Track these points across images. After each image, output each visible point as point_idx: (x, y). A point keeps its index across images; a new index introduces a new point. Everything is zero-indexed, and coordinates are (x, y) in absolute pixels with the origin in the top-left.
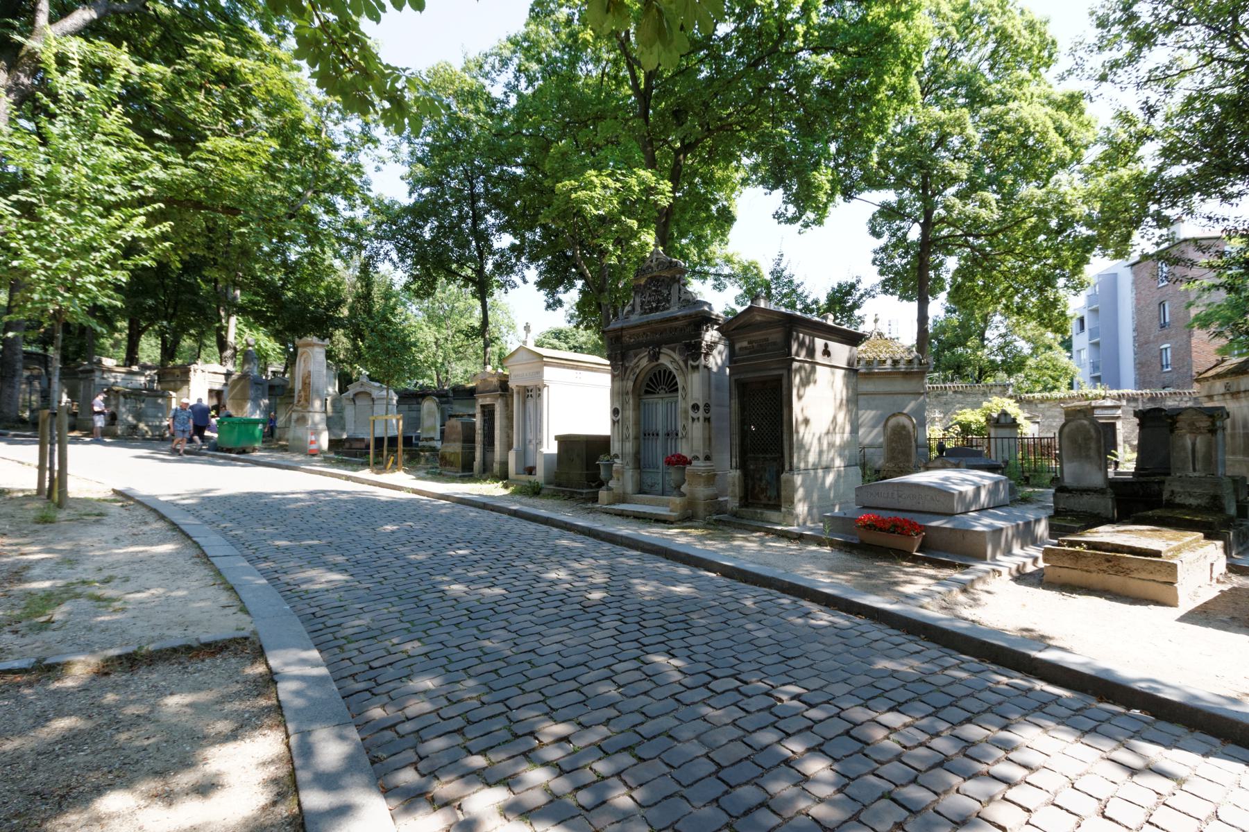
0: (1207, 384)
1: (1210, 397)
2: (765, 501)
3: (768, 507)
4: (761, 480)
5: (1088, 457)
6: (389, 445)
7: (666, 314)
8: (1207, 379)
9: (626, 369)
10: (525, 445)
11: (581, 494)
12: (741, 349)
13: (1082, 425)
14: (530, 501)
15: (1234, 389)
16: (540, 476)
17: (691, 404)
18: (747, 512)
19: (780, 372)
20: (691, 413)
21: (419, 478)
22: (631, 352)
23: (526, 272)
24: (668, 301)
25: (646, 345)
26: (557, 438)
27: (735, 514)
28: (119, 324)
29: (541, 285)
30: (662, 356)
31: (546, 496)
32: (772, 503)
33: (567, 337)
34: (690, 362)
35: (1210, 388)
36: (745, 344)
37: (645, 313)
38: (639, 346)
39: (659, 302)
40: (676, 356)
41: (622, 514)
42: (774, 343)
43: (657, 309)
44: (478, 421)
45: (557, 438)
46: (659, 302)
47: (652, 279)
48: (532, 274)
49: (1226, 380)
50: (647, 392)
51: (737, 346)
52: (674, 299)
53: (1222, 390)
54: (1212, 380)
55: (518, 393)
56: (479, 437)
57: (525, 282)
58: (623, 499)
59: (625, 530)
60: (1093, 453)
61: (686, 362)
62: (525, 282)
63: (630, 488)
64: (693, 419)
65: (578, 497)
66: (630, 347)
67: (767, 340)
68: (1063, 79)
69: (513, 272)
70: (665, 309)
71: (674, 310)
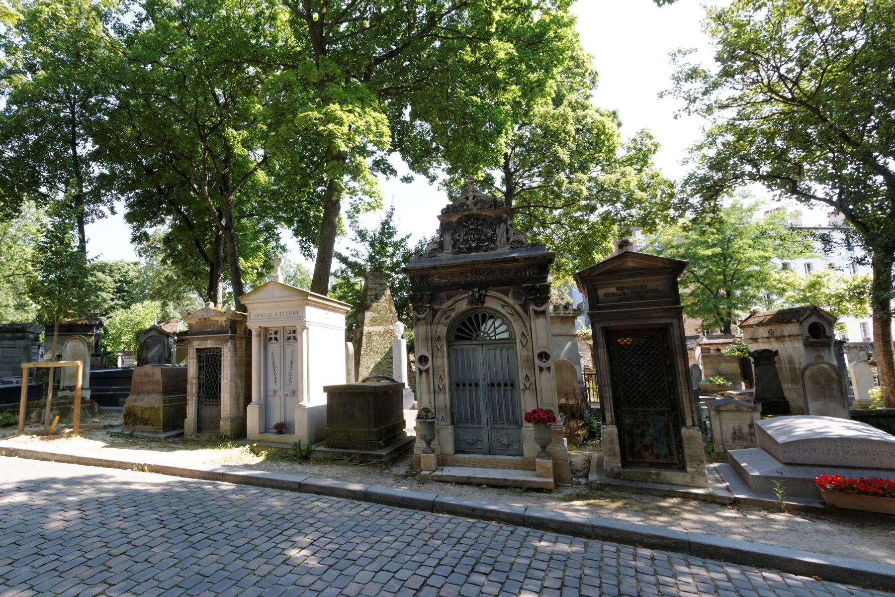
0: (750, 330)
1: (755, 340)
2: (651, 459)
3: (669, 466)
4: (643, 435)
5: (832, 397)
6: (29, 398)
7: (490, 255)
8: (751, 326)
9: (435, 312)
10: (266, 396)
11: (381, 457)
12: (606, 295)
13: (823, 369)
14: (298, 467)
15: (778, 334)
16: (301, 432)
17: (536, 352)
18: (634, 472)
19: (669, 321)
20: (537, 362)
21: (112, 445)
22: (443, 294)
23: (116, 203)
24: (494, 242)
25: (467, 287)
26: (327, 389)
27: (617, 476)
28: (885, 187)
29: (129, 218)
30: (487, 300)
31: (318, 461)
32: (662, 461)
33: (111, 271)
34: (532, 307)
35: (753, 332)
36: (613, 290)
37: (460, 251)
38: (454, 288)
39: (480, 241)
40: (510, 300)
41: (444, 481)
42: (655, 291)
43: (477, 249)
44: (192, 366)
45: (327, 389)
46: (480, 241)
47: (468, 218)
48: (121, 206)
49: (769, 327)
50: (458, 338)
51: (601, 292)
52: (501, 238)
53: (767, 335)
54: (755, 327)
55: (259, 335)
56: (192, 388)
57: (113, 212)
58: (442, 462)
59: (451, 496)
60: (836, 393)
61: (525, 307)
62: (113, 212)
63: (449, 448)
64: (541, 369)
65: (375, 460)
66: (439, 288)
67: (645, 287)
68: (661, 97)
69: (102, 201)
70: (488, 249)
71: (503, 251)
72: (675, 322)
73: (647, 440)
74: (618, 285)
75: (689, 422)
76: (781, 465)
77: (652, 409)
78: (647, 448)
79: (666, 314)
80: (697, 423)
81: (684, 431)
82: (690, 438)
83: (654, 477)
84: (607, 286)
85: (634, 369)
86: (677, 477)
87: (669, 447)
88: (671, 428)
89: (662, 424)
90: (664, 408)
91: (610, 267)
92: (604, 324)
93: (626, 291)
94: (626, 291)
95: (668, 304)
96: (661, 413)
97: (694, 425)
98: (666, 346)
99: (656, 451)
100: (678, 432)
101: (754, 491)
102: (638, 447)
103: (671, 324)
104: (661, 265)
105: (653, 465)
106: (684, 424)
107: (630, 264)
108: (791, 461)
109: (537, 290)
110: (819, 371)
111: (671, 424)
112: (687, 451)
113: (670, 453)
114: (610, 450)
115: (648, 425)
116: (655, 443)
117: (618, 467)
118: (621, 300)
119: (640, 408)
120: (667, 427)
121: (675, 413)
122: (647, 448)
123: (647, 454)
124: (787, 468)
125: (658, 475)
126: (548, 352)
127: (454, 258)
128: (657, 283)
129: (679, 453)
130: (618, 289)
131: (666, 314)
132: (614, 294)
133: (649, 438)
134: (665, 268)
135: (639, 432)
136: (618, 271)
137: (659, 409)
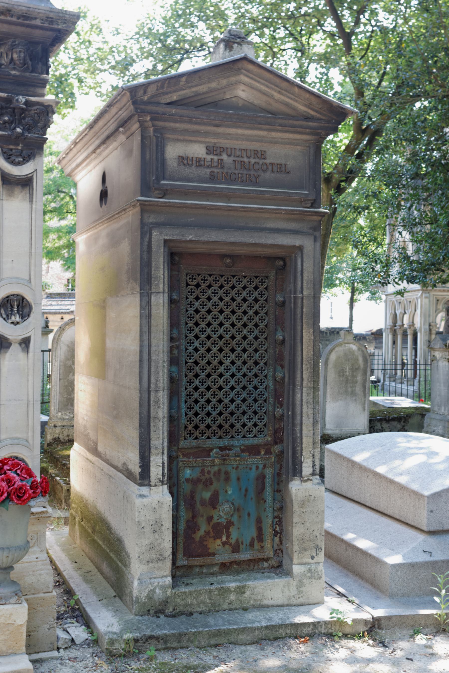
2: (225, 556)
3: (253, 566)
4: (214, 502)
12: (183, 160)
19: (296, 241)
32: (244, 556)
36: (197, 150)
42: (280, 168)
51: (173, 151)
67: (262, 155)
72: (308, 244)
73: (222, 512)
74: (212, 140)
75: (307, 469)
76: (421, 537)
77: (238, 442)
78: (218, 530)
79: (293, 226)
80: (318, 471)
81: (296, 487)
82: (307, 501)
83: (232, 597)
84: (188, 137)
85: (215, 350)
86: (270, 589)
87: (259, 521)
88: (269, 482)
89: (253, 474)
90: (260, 440)
91: (203, 88)
92: (171, 234)
93: (224, 157)
94: (224, 157)
95: (300, 202)
96: (253, 450)
97: (313, 474)
98: (280, 298)
99: (234, 535)
100: (280, 489)
101: (393, 597)
102: (204, 528)
103: (300, 249)
104: (302, 108)
105: (225, 567)
106: (297, 472)
107: (243, 92)
108: (439, 528)
109: (19, 115)
110: (346, 355)
111: (269, 472)
112: (297, 531)
113: (260, 537)
114: (151, 547)
115: (227, 479)
116: (235, 519)
117: (163, 588)
118: (212, 178)
119: (215, 442)
120: (261, 478)
121: (277, 448)
122: (218, 530)
123: (216, 545)
124: (432, 540)
125: (241, 590)
126: (29, 297)
127: (222, 582)
128: (283, 149)
129: (276, 533)
130: (210, 150)
131: (293, 226)
132: (199, 162)
133: (226, 507)
134: (308, 118)
135: (207, 495)
136: (215, 104)
137: (250, 441)
